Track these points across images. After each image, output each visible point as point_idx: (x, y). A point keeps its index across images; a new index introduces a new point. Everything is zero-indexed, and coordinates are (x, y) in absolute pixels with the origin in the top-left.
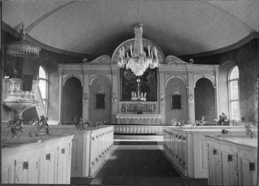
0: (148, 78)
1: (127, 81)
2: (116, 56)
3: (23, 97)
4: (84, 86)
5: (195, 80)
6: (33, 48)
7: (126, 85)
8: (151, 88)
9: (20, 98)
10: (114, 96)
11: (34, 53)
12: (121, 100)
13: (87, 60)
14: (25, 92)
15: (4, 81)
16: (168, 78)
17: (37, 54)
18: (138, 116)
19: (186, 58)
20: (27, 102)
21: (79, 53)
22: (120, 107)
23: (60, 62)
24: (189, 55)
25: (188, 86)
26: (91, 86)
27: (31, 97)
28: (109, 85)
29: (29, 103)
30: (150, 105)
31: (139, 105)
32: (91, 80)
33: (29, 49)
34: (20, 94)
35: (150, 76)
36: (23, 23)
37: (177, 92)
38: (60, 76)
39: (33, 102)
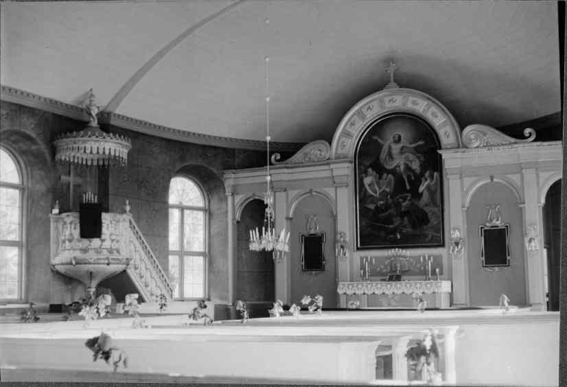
0: (421, 189)
1: (373, 200)
2: (341, 142)
3: (85, 251)
4: (338, 215)
5: (543, 186)
6: (102, 143)
7: (370, 209)
8: (429, 215)
9: (78, 254)
10: (342, 239)
11: (112, 154)
12: (358, 249)
13: (279, 157)
14: (90, 242)
15: (52, 220)
16: (548, 179)
17: (122, 158)
18: (389, 286)
19: (514, 130)
20: (90, 263)
21: (253, 141)
22: (357, 262)
23: (229, 167)
24: (521, 123)
25: (524, 203)
26: (291, 219)
27: (115, 251)
28: (332, 213)
29: (94, 264)
30: (367, 258)
31: (401, 259)
32: (292, 203)
33: (106, 147)
34: (81, 246)
35: (426, 183)
36: (91, 90)
37: (497, 220)
38: (230, 199)
39: (107, 261)
